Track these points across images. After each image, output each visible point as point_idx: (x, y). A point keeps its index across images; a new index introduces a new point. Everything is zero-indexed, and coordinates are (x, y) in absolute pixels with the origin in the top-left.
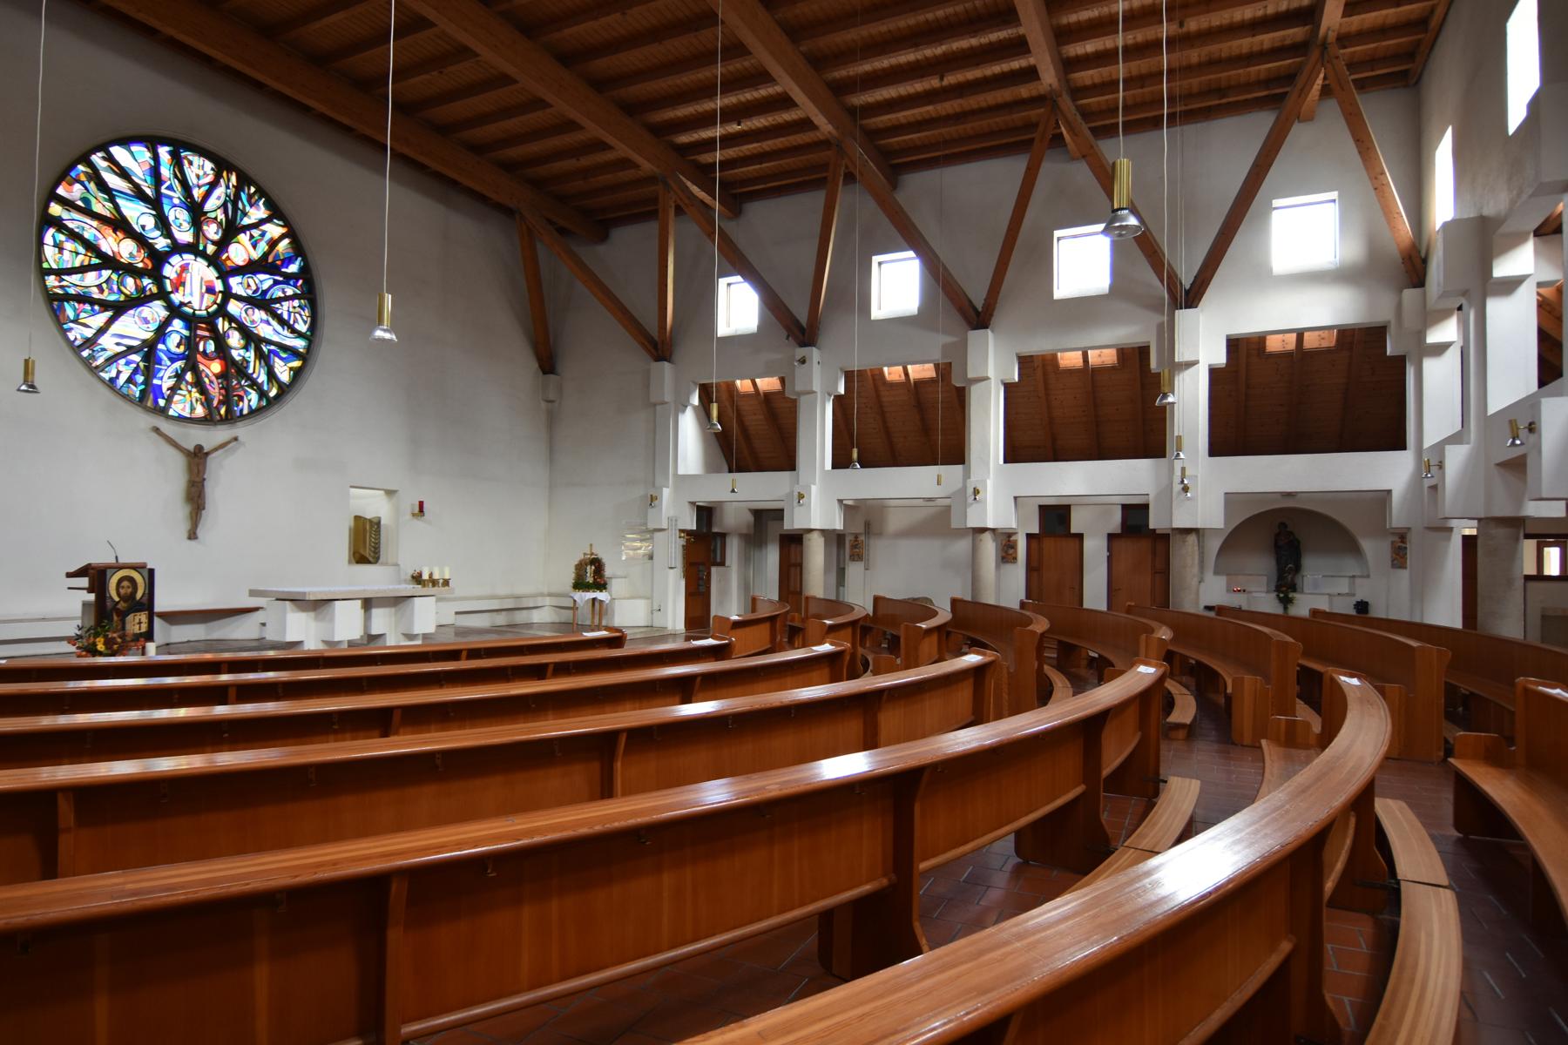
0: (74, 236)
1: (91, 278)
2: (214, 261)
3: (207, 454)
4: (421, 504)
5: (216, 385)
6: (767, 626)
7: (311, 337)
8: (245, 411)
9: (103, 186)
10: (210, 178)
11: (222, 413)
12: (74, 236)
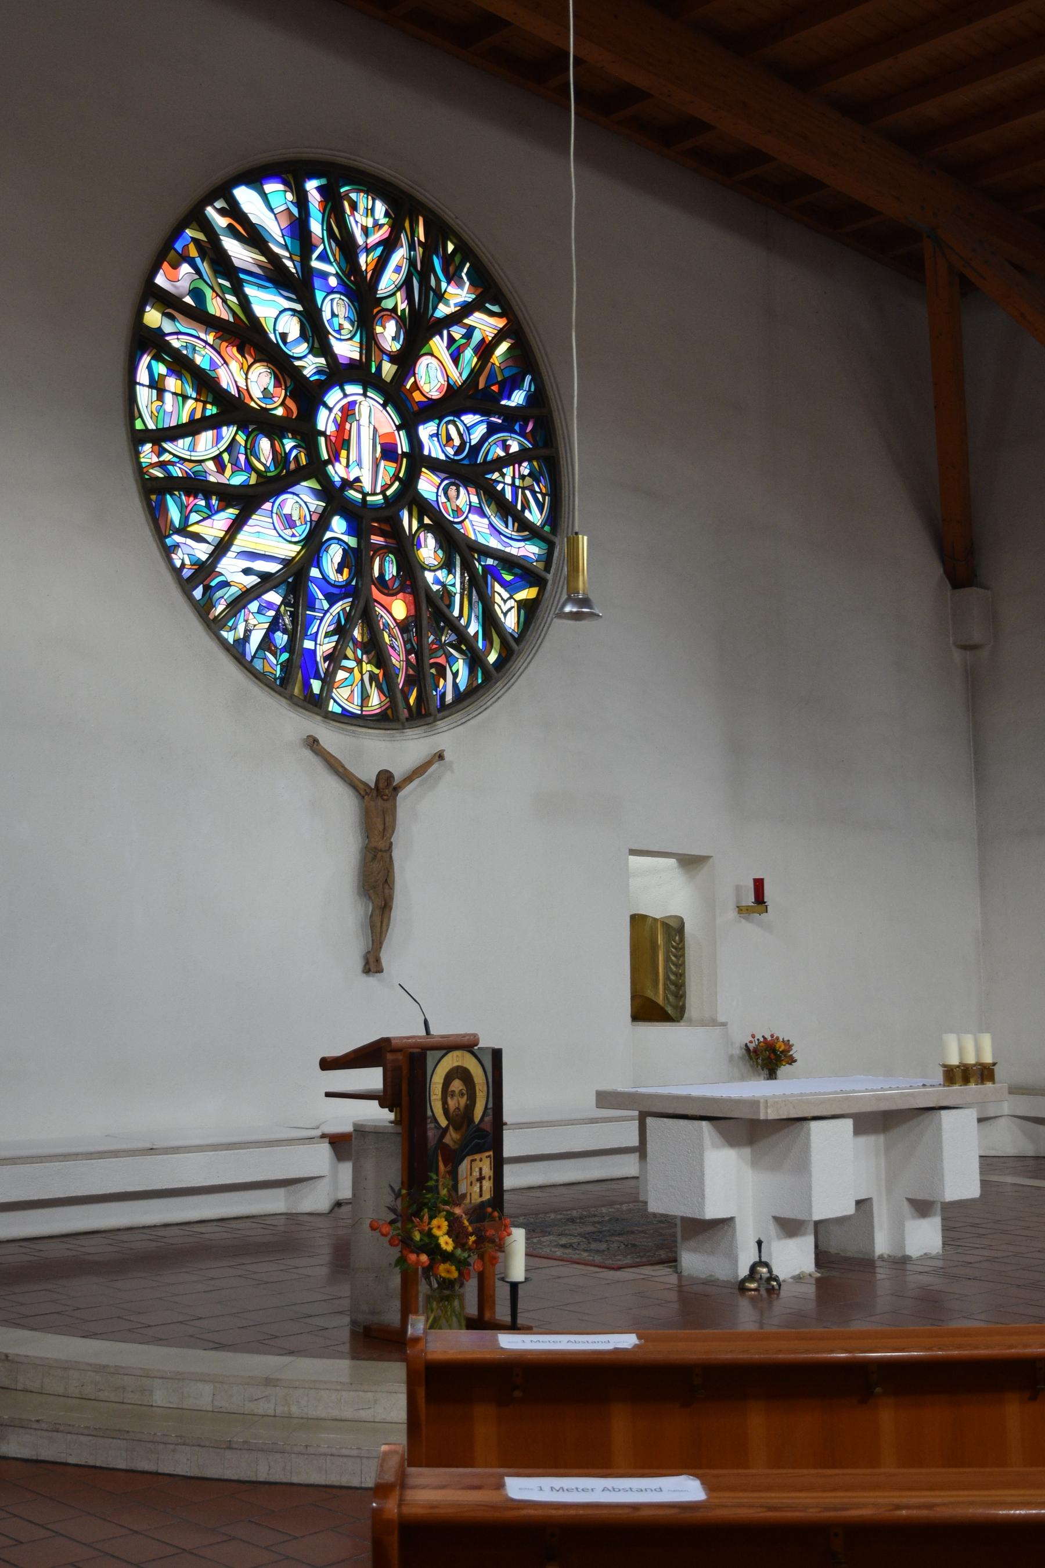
0: (181, 364)
1: (206, 444)
4: (759, 885)
8: (449, 698)
9: (223, 264)
10: (383, 233)
11: (412, 704)
12: (181, 364)
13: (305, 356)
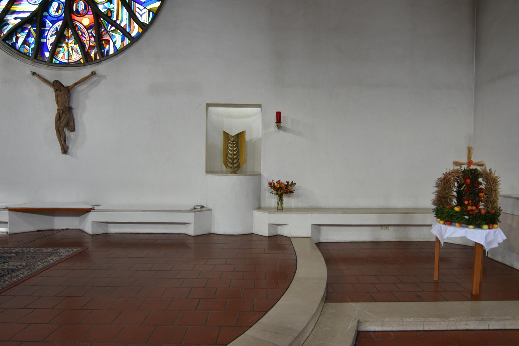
6: (262, 205)
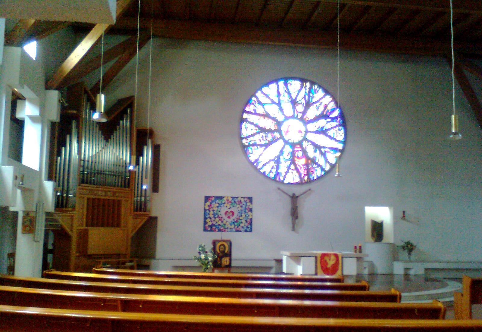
1: (258, 137)
2: (302, 119)
3: (297, 197)
5: (302, 169)
7: (344, 143)
13: (284, 114)
